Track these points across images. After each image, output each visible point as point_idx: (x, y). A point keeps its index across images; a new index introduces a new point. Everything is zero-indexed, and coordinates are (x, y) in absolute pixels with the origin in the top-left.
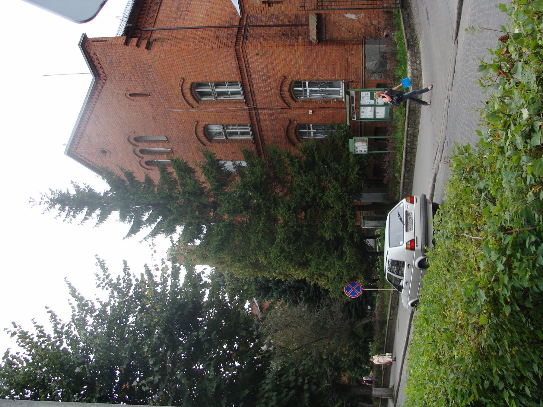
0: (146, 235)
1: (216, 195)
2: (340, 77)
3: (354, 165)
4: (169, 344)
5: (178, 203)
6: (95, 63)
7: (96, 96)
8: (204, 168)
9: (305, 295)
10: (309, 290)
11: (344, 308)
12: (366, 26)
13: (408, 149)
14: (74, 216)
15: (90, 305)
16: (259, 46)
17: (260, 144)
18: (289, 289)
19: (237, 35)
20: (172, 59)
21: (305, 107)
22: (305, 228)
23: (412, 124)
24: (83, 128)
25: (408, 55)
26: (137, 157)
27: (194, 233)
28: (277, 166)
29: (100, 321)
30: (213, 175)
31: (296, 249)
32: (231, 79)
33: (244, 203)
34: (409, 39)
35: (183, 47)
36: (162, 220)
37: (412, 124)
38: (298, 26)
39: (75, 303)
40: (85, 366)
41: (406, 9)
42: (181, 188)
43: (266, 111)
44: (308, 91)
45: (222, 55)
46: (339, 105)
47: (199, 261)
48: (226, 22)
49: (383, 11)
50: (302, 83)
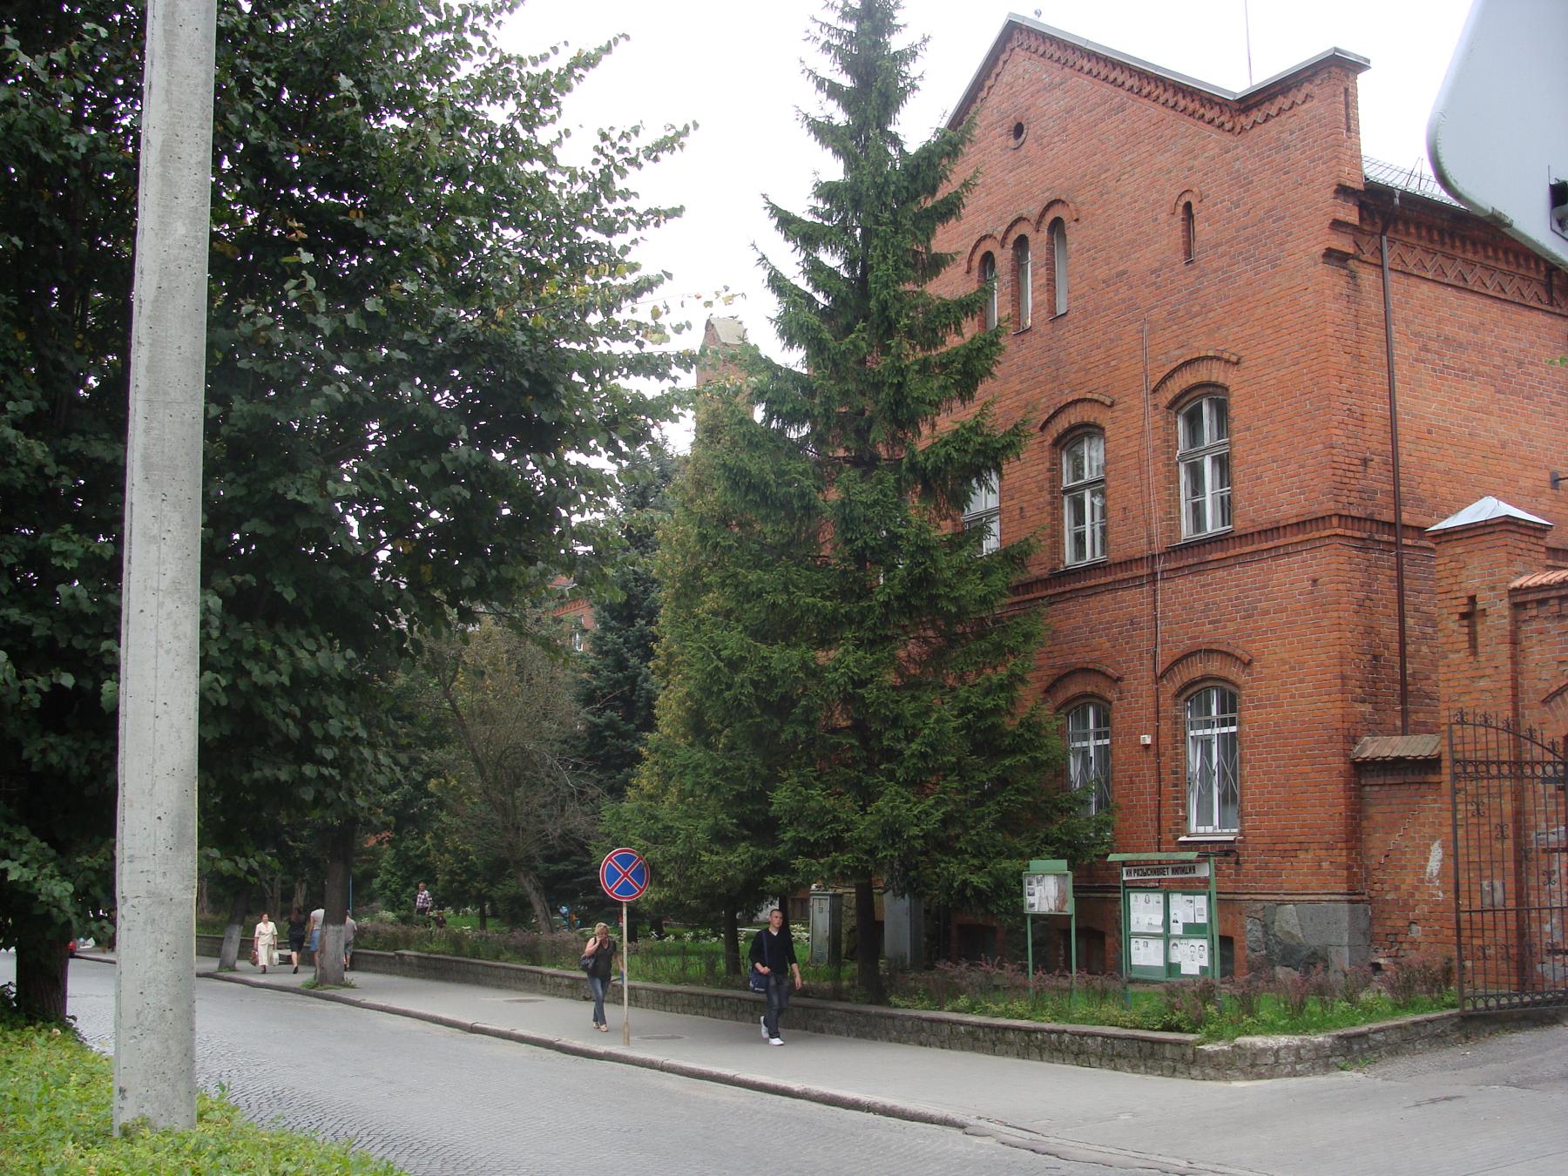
0: (773, 261)
1: (895, 464)
3: (990, 873)
4: (430, 355)
5: (870, 353)
6: (1280, 98)
7: (1182, 103)
8: (975, 429)
9: (611, 725)
10: (624, 736)
11: (574, 839)
12: (1406, 903)
13: (1039, 1036)
14: (827, 47)
15: (546, 113)
16: (1341, 586)
17: (1050, 592)
18: (627, 678)
19: (1372, 520)
21: (1162, 722)
22: (801, 731)
23: (1113, 1048)
25: (1320, 1038)
26: (1005, 227)
27: (783, 403)
28: (984, 645)
29: (500, 145)
30: (955, 455)
31: (740, 705)
32: (1241, 504)
33: (873, 548)
34: (1368, 1039)
35: (1333, 359)
36: (821, 307)
37: (1113, 1048)
38: (1403, 702)
39: (556, 64)
40: (358, 107)
41: (1460, 1029)
42: (916, 362)
43: (1148, 609)
44: (1208, 731)
45: (1313, 475)
46: (1167, 827)
47: (703, 417)
48: (1410, 486)
49: (1450, 960)
50: (1106, 729)
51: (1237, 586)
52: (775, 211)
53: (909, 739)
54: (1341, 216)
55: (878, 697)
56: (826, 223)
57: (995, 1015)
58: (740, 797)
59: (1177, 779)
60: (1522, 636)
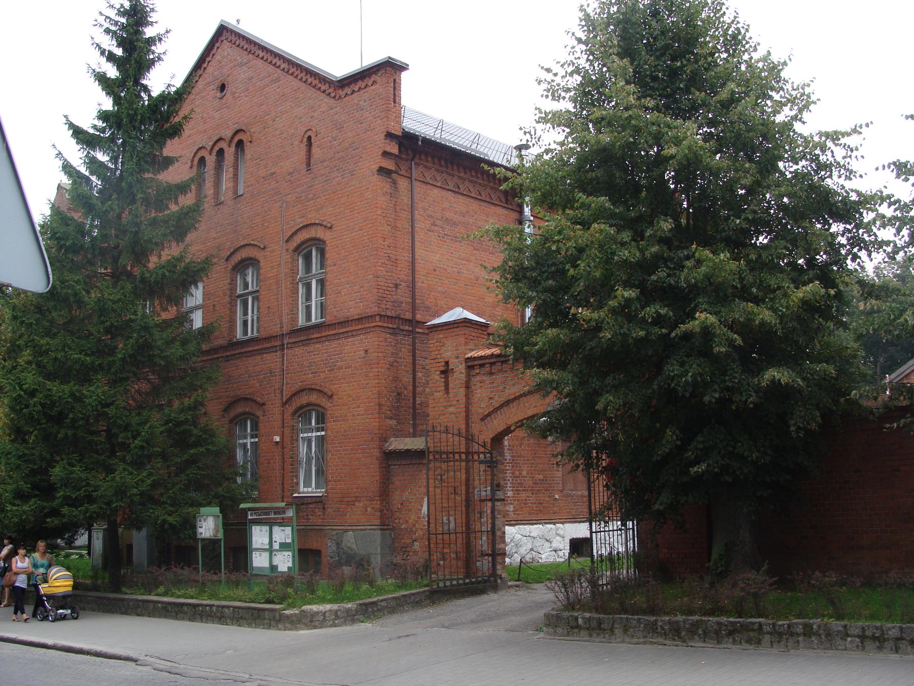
0: (66, 156)
2: (331, 489)
7: (310, 80)
8: (180, 259)
14: (107, 31)
17: (228, 354)
19: (399, 318)
20: (363, 210)
21: (285, 429)
22: (70, 433)
23: (239, 614)
24: (261, 55)
25: (350, 605)
26: (212, 143)
28: (182, 384)
30: (167, 274)
31: (33, 417)
33: (116, 327)
35: (380, 228)
38: (414, 419)
41: (429, 598)
44: (310, 435)
45: (366, 292)
50: (323, 425)
51: (326, 353)
52: (71, 126)
53: (134, 438)
54: (388, 149)
55: (116, 414)
56: (102, 135)
57: (179, 597)
58: (33, 472)
59: (293, 461)
60: (472, 384)
